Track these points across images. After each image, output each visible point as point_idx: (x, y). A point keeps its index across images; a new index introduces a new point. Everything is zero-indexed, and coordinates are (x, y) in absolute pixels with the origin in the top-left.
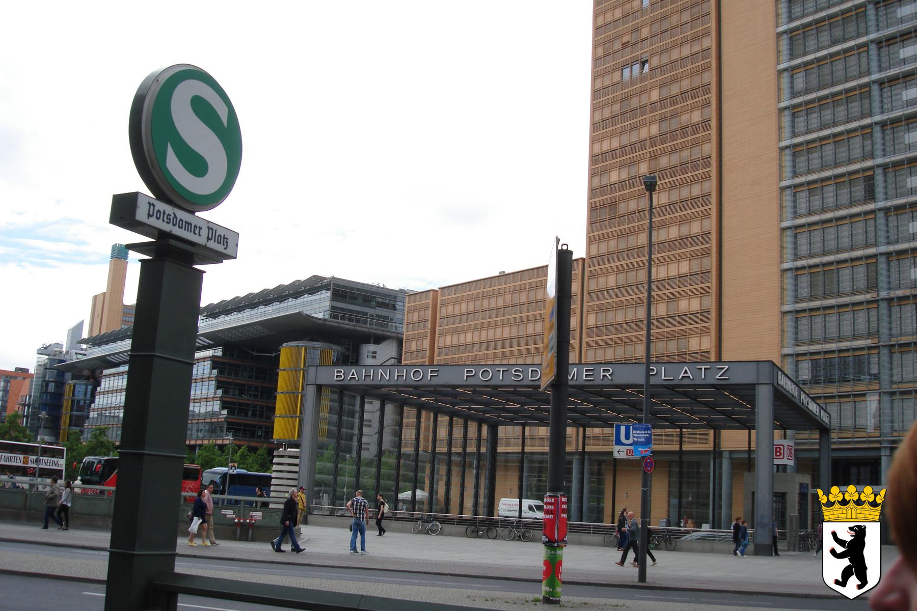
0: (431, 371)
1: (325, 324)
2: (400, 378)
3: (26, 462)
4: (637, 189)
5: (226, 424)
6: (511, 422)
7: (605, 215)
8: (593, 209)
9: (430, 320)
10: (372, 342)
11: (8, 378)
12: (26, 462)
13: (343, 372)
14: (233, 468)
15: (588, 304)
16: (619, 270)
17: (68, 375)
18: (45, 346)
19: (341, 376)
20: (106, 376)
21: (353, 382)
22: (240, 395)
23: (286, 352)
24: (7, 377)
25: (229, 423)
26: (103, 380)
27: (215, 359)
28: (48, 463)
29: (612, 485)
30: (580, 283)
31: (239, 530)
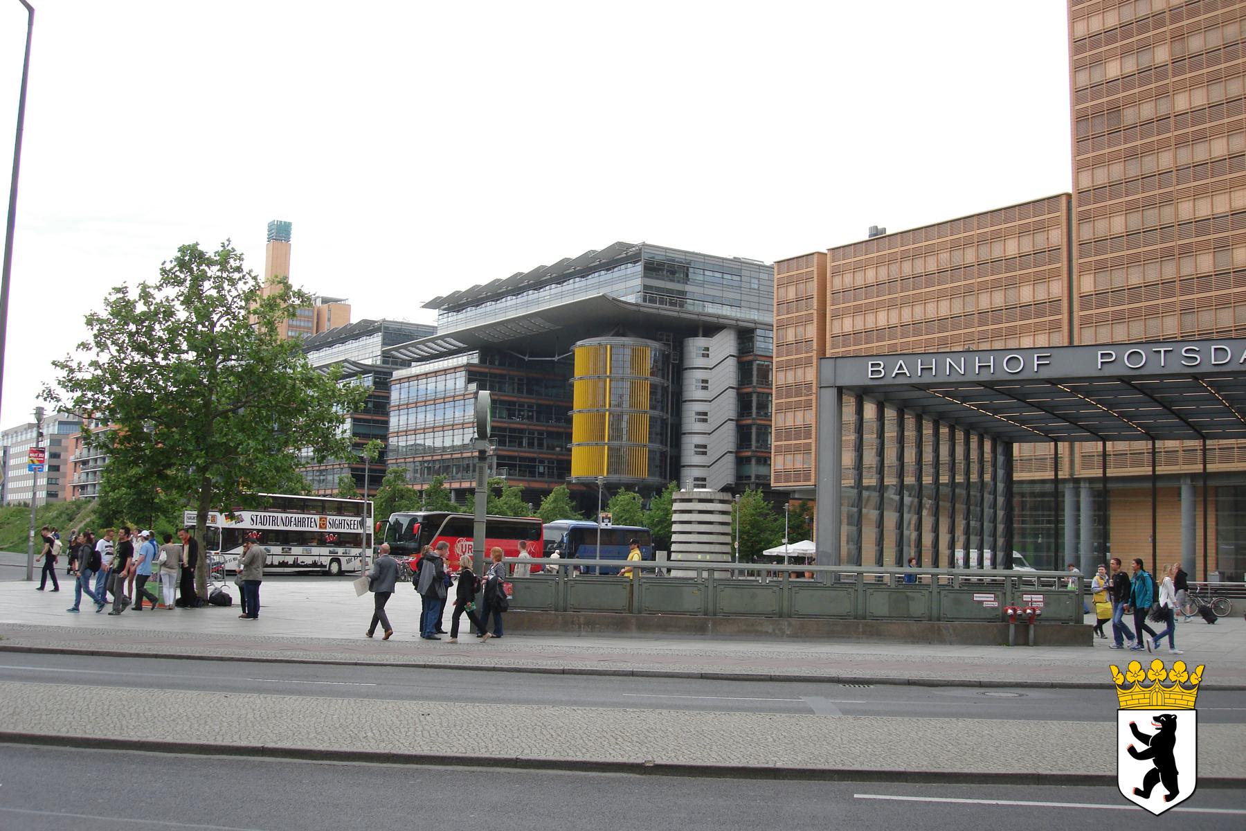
1: (639, 311)
2: (983, 370)
3: (323, 525)
4: (1153, 86)
5: (495, 458)
7: (1101, 126)
8: (1080, 119)
9: (815, 296)
10: (701, 335)
12: (323, 525)
13: (882, 366)
16: (1130, 208)
22: (510, 417)
23: (583, 351)
25: (499, 457)
28: (347, 524)
29: (1151, 521)
30: (1065, 230)
31: (1012, 627)
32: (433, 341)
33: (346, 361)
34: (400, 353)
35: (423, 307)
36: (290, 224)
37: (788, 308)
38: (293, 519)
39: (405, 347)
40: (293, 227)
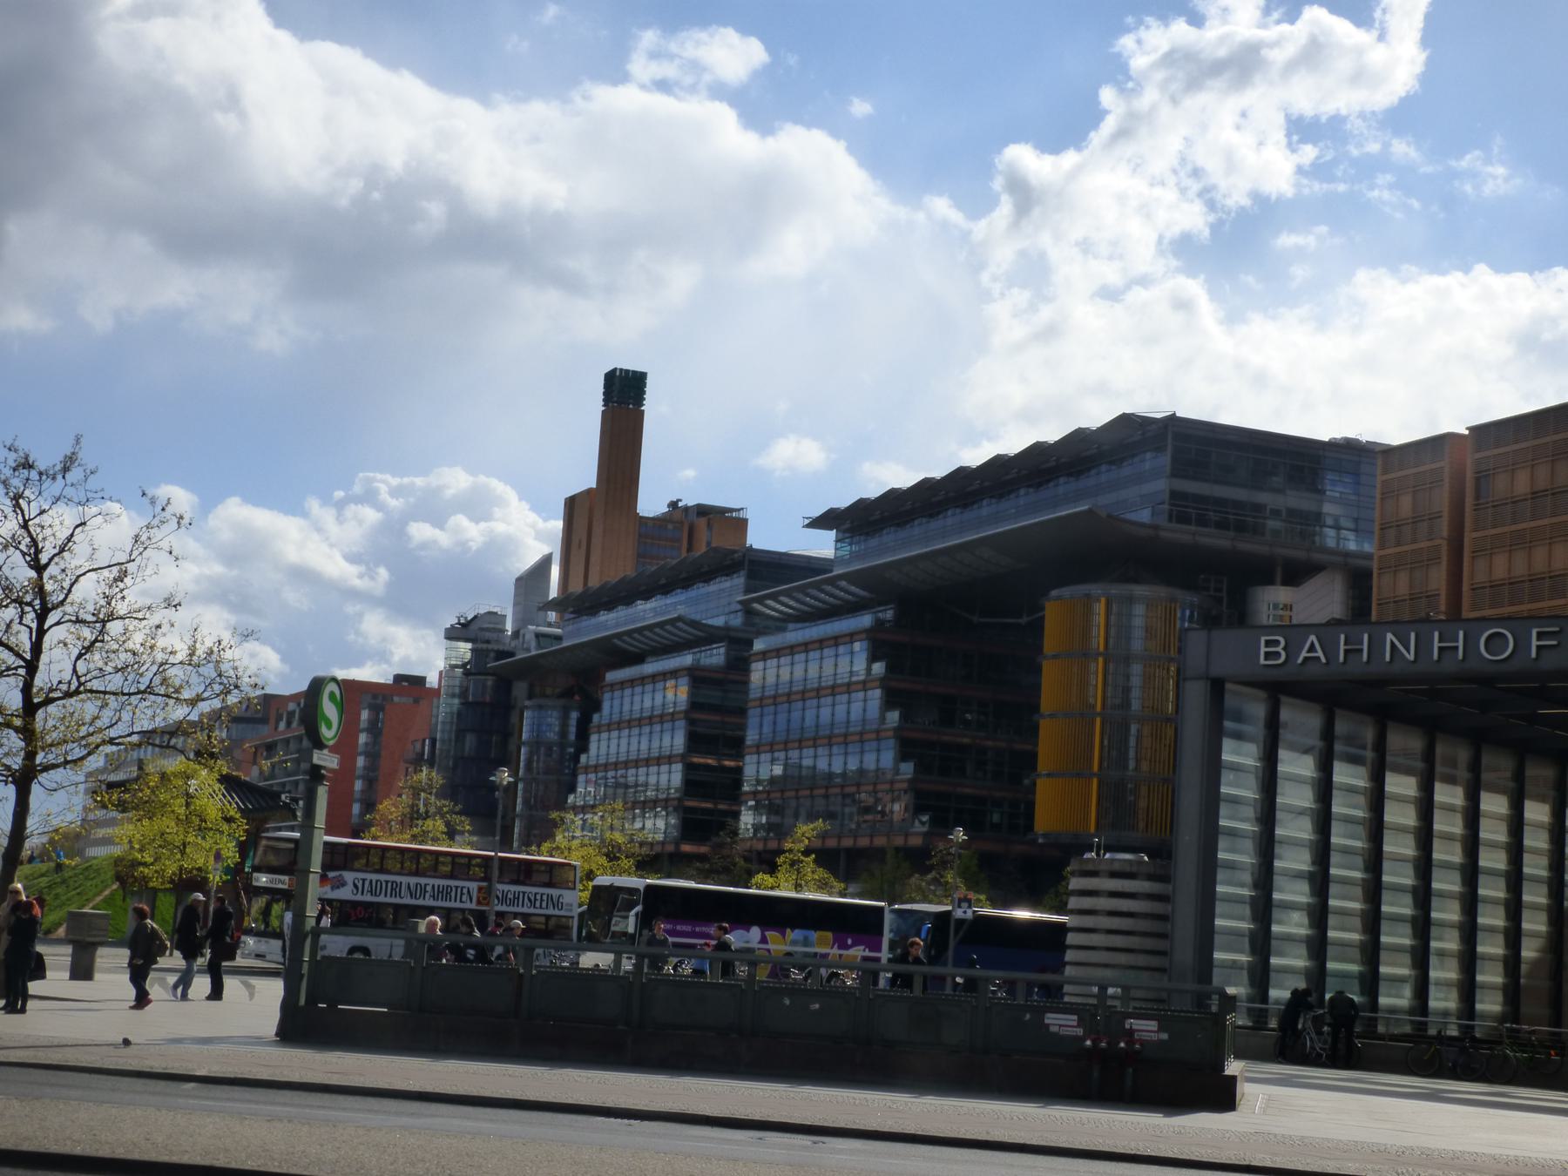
0: (1540, 636)
10: (1279, 579)
17: (520, 689)
18: (462, 621)
19: (1277, 654)
20: (764, 655)
24: (375, 697)
33: (679, 619)
39: (774, 597)
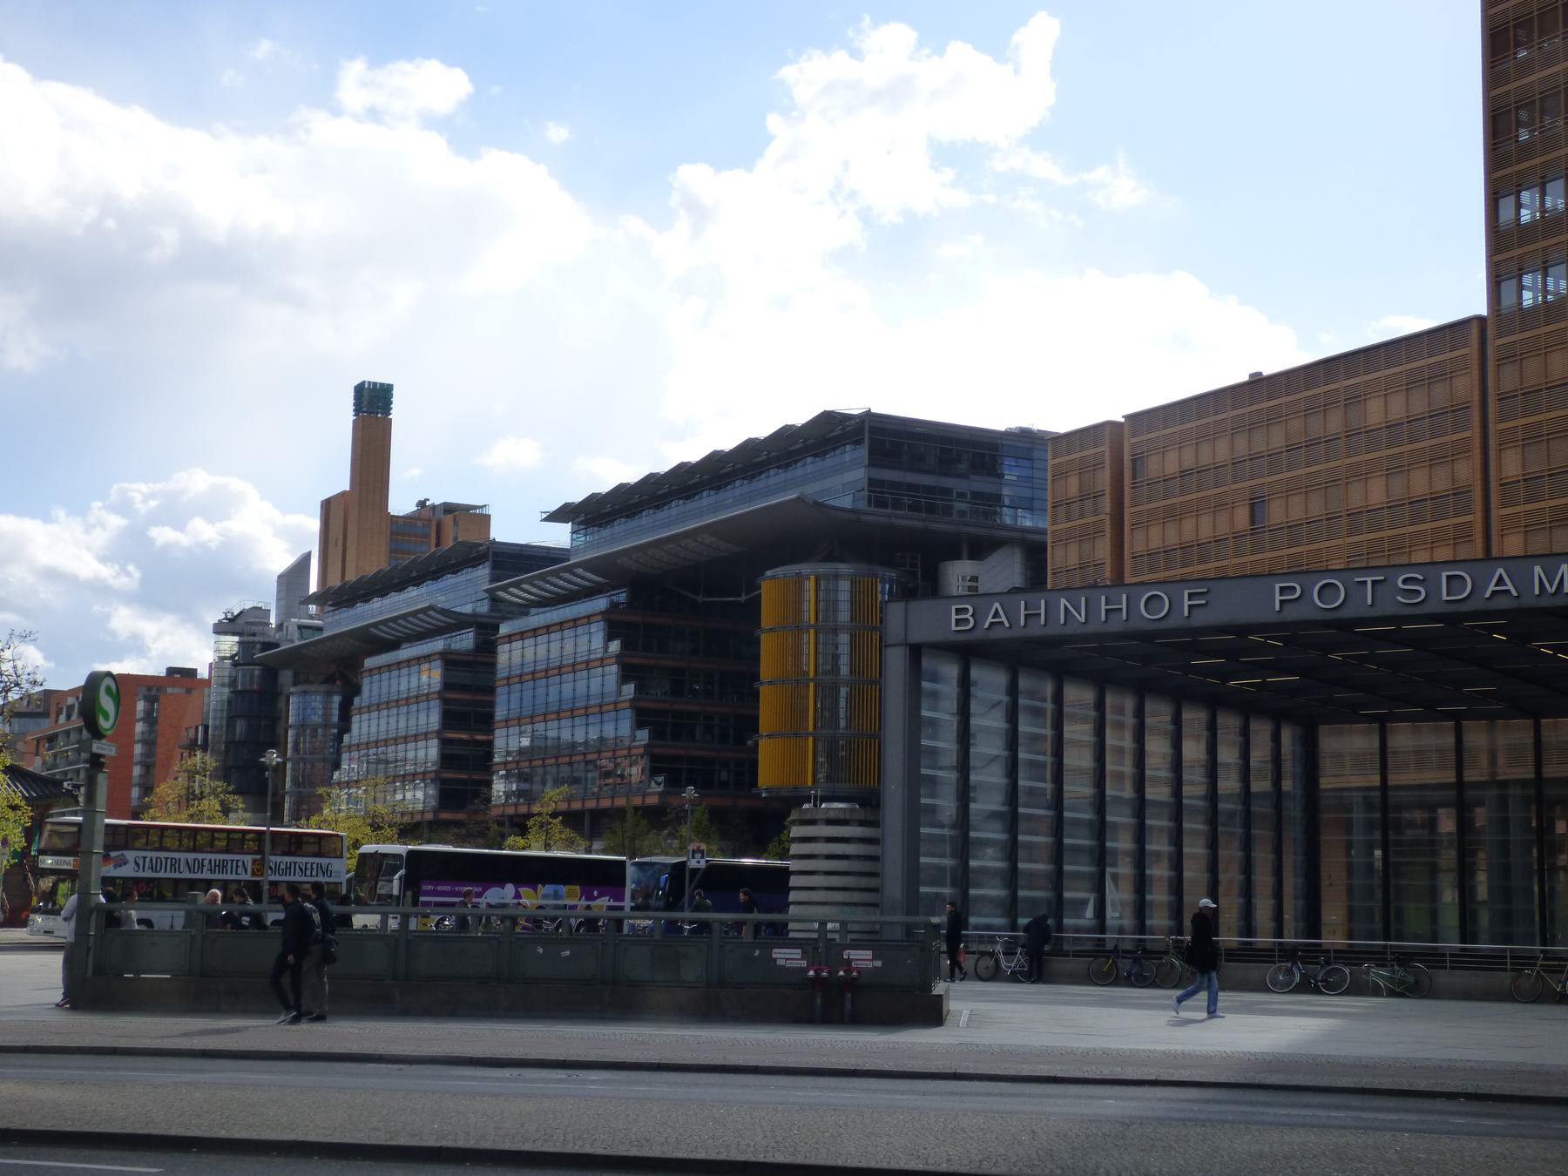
0: (1191, 596)
2: (1113, 616)
6: (1348, 715)
9: (1108, 492)
11: (154, 693)
14: (698, 856)
15: (1502, 426)
18: (229, 616)
20: (510, 638)
21: (998, 634)
23: (771, 588)
24: (149, 689)
26: (366, 681)
27: (450, 657)
32: (570, 569)
33: (431, 608)
34: (509, 593)
35: (546, 520)
36: (392, 386)
37: (1068, 513)
38: (206, 863)
40: (395, 392)
